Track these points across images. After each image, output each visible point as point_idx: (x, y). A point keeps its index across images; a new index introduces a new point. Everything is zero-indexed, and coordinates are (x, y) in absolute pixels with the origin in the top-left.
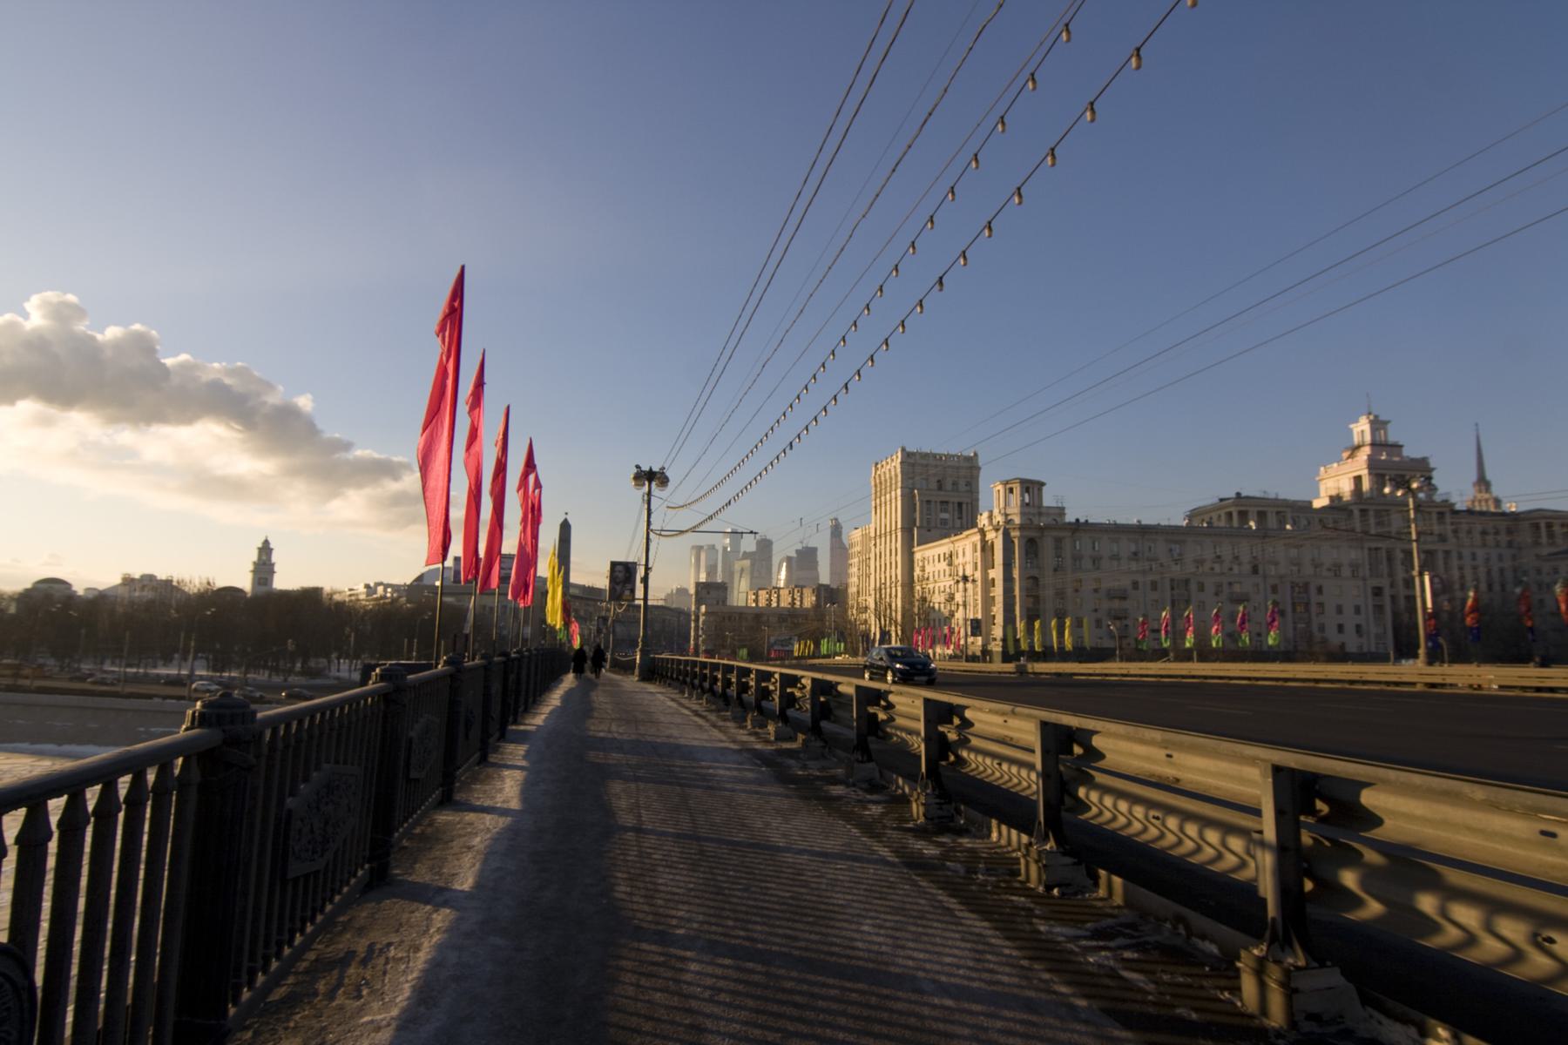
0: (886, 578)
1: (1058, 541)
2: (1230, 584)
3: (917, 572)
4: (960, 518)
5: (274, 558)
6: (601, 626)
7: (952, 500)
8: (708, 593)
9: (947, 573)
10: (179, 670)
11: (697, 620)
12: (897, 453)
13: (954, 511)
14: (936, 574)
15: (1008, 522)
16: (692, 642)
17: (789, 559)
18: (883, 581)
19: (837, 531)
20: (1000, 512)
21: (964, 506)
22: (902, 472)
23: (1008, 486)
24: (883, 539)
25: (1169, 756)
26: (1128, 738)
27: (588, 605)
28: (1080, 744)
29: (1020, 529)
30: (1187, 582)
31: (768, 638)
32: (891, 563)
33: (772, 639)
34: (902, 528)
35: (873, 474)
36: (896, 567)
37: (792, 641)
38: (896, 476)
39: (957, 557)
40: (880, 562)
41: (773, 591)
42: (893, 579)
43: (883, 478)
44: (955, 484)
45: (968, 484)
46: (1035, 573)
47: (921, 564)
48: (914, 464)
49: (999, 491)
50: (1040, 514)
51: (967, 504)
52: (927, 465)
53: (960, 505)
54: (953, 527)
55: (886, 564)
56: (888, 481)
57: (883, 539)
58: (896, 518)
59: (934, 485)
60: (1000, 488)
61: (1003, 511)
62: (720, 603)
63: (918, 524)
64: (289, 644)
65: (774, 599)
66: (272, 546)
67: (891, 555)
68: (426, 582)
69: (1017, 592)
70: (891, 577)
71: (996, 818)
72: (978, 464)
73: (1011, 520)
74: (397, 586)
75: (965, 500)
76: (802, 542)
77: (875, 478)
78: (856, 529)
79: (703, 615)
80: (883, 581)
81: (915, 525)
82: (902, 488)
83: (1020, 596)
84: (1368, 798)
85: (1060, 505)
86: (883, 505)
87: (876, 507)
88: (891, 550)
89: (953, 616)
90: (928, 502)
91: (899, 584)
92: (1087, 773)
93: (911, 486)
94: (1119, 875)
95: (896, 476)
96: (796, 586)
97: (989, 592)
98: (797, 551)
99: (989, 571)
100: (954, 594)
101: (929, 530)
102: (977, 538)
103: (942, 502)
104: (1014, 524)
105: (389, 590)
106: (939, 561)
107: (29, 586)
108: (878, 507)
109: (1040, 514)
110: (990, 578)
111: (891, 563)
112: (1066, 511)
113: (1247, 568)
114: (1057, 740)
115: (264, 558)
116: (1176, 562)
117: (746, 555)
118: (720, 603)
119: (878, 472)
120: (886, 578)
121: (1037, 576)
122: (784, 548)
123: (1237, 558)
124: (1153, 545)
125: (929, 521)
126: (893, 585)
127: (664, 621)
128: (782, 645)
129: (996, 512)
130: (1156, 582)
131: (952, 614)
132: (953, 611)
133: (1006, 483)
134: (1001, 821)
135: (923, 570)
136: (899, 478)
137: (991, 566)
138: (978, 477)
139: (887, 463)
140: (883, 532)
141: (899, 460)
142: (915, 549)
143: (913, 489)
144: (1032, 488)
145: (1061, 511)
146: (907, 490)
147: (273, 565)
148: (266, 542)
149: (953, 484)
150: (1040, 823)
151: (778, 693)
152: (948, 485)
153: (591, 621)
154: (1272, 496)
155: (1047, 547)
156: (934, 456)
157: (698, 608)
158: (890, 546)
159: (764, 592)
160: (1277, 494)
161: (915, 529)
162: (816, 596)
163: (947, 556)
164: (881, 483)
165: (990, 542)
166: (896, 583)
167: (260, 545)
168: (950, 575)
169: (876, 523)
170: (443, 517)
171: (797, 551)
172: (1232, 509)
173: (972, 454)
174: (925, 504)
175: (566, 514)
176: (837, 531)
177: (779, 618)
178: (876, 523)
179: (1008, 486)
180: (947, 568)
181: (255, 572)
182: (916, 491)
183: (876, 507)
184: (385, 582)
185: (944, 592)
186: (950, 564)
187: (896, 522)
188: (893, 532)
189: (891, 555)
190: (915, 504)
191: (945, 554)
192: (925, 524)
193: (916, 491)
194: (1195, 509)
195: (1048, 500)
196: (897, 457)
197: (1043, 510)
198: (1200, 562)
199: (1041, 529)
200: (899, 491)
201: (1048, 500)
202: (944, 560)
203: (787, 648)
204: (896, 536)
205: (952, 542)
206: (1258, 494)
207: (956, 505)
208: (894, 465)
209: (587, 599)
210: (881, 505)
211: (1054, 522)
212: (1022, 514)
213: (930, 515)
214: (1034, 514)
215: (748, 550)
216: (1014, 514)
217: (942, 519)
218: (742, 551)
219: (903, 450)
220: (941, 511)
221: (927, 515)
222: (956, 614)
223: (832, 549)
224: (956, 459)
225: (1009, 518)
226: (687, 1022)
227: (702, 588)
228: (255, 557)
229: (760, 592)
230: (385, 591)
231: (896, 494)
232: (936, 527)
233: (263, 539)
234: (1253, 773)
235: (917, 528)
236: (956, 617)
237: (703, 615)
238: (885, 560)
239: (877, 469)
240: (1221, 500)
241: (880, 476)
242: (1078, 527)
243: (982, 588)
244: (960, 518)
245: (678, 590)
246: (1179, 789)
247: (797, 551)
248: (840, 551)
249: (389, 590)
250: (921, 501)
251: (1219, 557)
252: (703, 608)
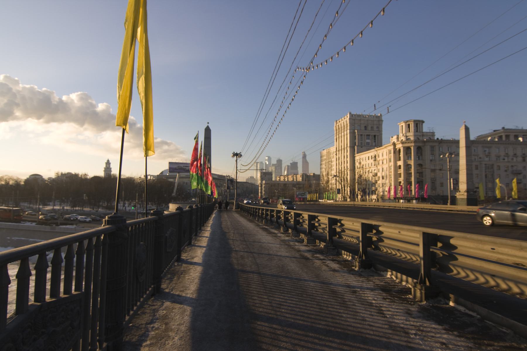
0: (342, 168)
1: (432, 148)
2: (512, 166)
3: (357, 164)
4: (375, 142)
5: (111, 166)
6: (230, 185)
7: (371, 134)
8: (265, 176)
9: (373, 164)
10: (53, 207)
11: (261, 186)
12: (347, 115)
13: (372, 139)
14: (367, 165)
15: (408, 139)
16: (260, 195)
17: (288, 166)
18: (340, 169)
19: (304, 156)
20: (403, 135)
21: (376, 137)
22: (350, 123)
23: (407, 123)
24: (340, 152)
25: (399, 232)
26: (408, 230)
27: (221, 182)
28: (375, 229)
29: (414, 142)
30: (493, 165)
31: (296, 193)
32: (344, 162)
33: (297, 193)
34: (350, 146)
35: (335, 126)
36: (347, 163)
37: (306, 194)
38: (347, 125)
39: (379, 157)
40: (339, 161)
41: (286, 176)
42: (346, 168)
43: (340, 127)
44: (372, 128)
45: (378, 128)
46: (420, 162)
47: (359, 161)
48: (355, 120)
49: (402, 126)
50: (423, 135)
51: (378, 136)
52: (360, 120)
53: (375, 136)
54: (372, 146)
55: (342, 162)
56: (340, 128)
57: (340, 152)
58: (347, 142)
59: (363, 128)
60: (404, 124)
61: (405, 135)
62: (270, 180)
63: (357, 144)
64: (84, 196)
65: (295, 178)
66: (110, 162)
67: (344, 158)
68: (164, 174)
69: (68, 226)
70: (344, 167)
71: (344, 250)
72: (382, 118)
73: (409, 138)
74: (155, 176)
75: (377, 134)
76: (292, 160)
77: (336, 127)
78: (324, 150)
79: (264, 184)
80: (340, 169)
81: (355, 144)
82: (350, 129)
83: (414, 173)
84: (452, 241)
85: (431, 131)
86: (340, 138)
87: (336, 139)
88: (344, 156)
89: (377, 182)
90: (361, 135)
91: (349, 170)
92: (455, 256)
93: (353, 129)
94: (394, 271)
95: (347, 125)
96: (294, 174)
97: (398, 171)
98: (291, 164)
99: (397, 162)
100: (377, 173)
101: (362, 147)
102: (392, 147)
103: (367, 135)
104: (411, 140)
105: (152, 177)
106: (369, 159)
107: (28, 177)
108: (338, 139)
109: (423, 135)
110: (398, 165)
111: (344, 162)
112: (435, 134)
113: (520, 159)
114: (366, 228)
115: (108, 166)
116: (487, 156)
117: (273, 165)
118: (270, 180)
119: (337, 125)
120: (342, 168)
121: (422, 163)
122: (286, 163)
123: (515, 154)
124: (476, 149)
125: (361, 144)
126: (346, 170)
127: (247, 187)
128: (302, 196)
129: (401, 135)
130: (477, 165)
131: (376, 182)
132: (377, 181)
133: (406, 122)
134: (345, 251)
135: (360, 163)
136: (349, 125)
137: (398, 159)
138: (382, 125)
139: (342, 120)
140: (340, 149)
141: (348, 118)
142: (356, 155)
143: (355, 130)
144: (418, 124)
145: (433, 134)
146: (352, 130)
147: (111, 168)
148: (108, 161)
149: (371, 128)
150: (422, 274)
151: (328, 229)
152: (369, 128)
153: (222, 187)
154: (520, 128)
155: (427, 150)
156: (363, 115)
157: (262, 182)
158: (344, 154)
159: (283, 177)
160: (522, 127)
161: (356, 147)
162: (302, 178)
163: (373, 157)
164: (339, 129)
165: (398, 149)
166: (347, 170)
167: (106, 162)
168: (375, 165)
169: (336, 146)
170: (151, 134)
171: (291, 164)
172: (502, 134)
173: (379, 115)
174: (360, 136)
175: (208, 123)
176: (304, 156)
177: (293, 185)
178: (336, 146)
179: (407, 123)
180: (373, 162)
181: (105, 171)
182: (356, 131)
183: (336, 139)
184: (151, 175)
185: (371, 172)
186: (375, 160)
187: (347, 144)
188: (346, 149)
189: (344, 158)
190: (356, 136)
191: (372, 156)
192: (360, 145)
193: (356, 131)
194: (479, 136)
195: (426, 129)
196: (347, 117)
197: (425, 134)
198: (498, 157)
199: (424, 142)
200: (348, 131)
201: (426, 129)
202: (372, 159)
203: (303, 197)
204: (347, 150)
205: (376, 151)
206: (513, 128)
207: (373, 136)
208: (346, 119)
209: (220, 179)
210: (339, 138)
211: (430, 139)
212: (415, 136)
213: (362, 140)
214: (420, 136)
215: (274, 163)
216: (410, 136)
217: (367, 142)
218: (272, 163)
219: (350, 113)
220: (367, 139)
221: (361, 140)
222: (378, 182)
223: (303, 162)
224: (372, 117)
225: (408, 138)
226: (256, 325)
227: (263, 174)
228: (104, 166)
229: (281, 177)
230: (151, 177)
231: (347, 133)
232: (365, 146)
233: (107, 160)
234: (418, 235)
235: (357, 146)
236: (378, 183)
237: (264, 184)
238: (341, 160)
239: (337, 123)
240: (494, 131)
241: (338, 126)
242: (441, 142)
243: (394, 170)
244: (375, 142)
245: (250, 177)
246: (501, 263)
247: (291, 164)
248: (305, 163)
249: (152, 177)
250: (358, 135)
251: (507, 154)
252: (264, 182)
